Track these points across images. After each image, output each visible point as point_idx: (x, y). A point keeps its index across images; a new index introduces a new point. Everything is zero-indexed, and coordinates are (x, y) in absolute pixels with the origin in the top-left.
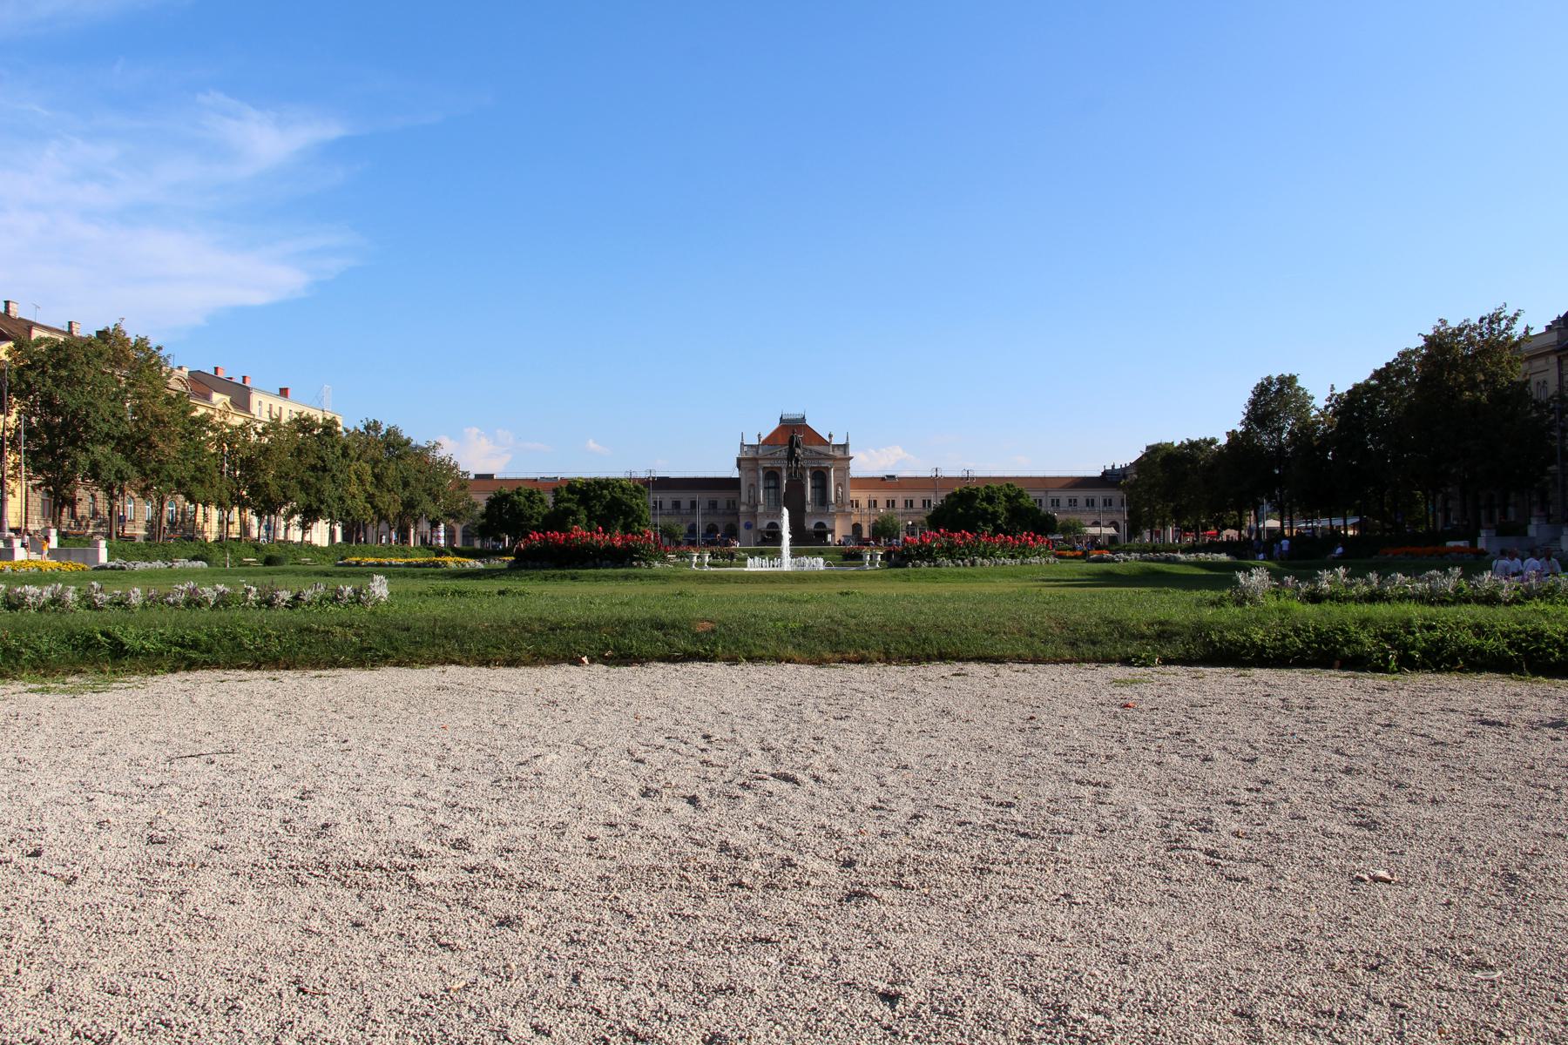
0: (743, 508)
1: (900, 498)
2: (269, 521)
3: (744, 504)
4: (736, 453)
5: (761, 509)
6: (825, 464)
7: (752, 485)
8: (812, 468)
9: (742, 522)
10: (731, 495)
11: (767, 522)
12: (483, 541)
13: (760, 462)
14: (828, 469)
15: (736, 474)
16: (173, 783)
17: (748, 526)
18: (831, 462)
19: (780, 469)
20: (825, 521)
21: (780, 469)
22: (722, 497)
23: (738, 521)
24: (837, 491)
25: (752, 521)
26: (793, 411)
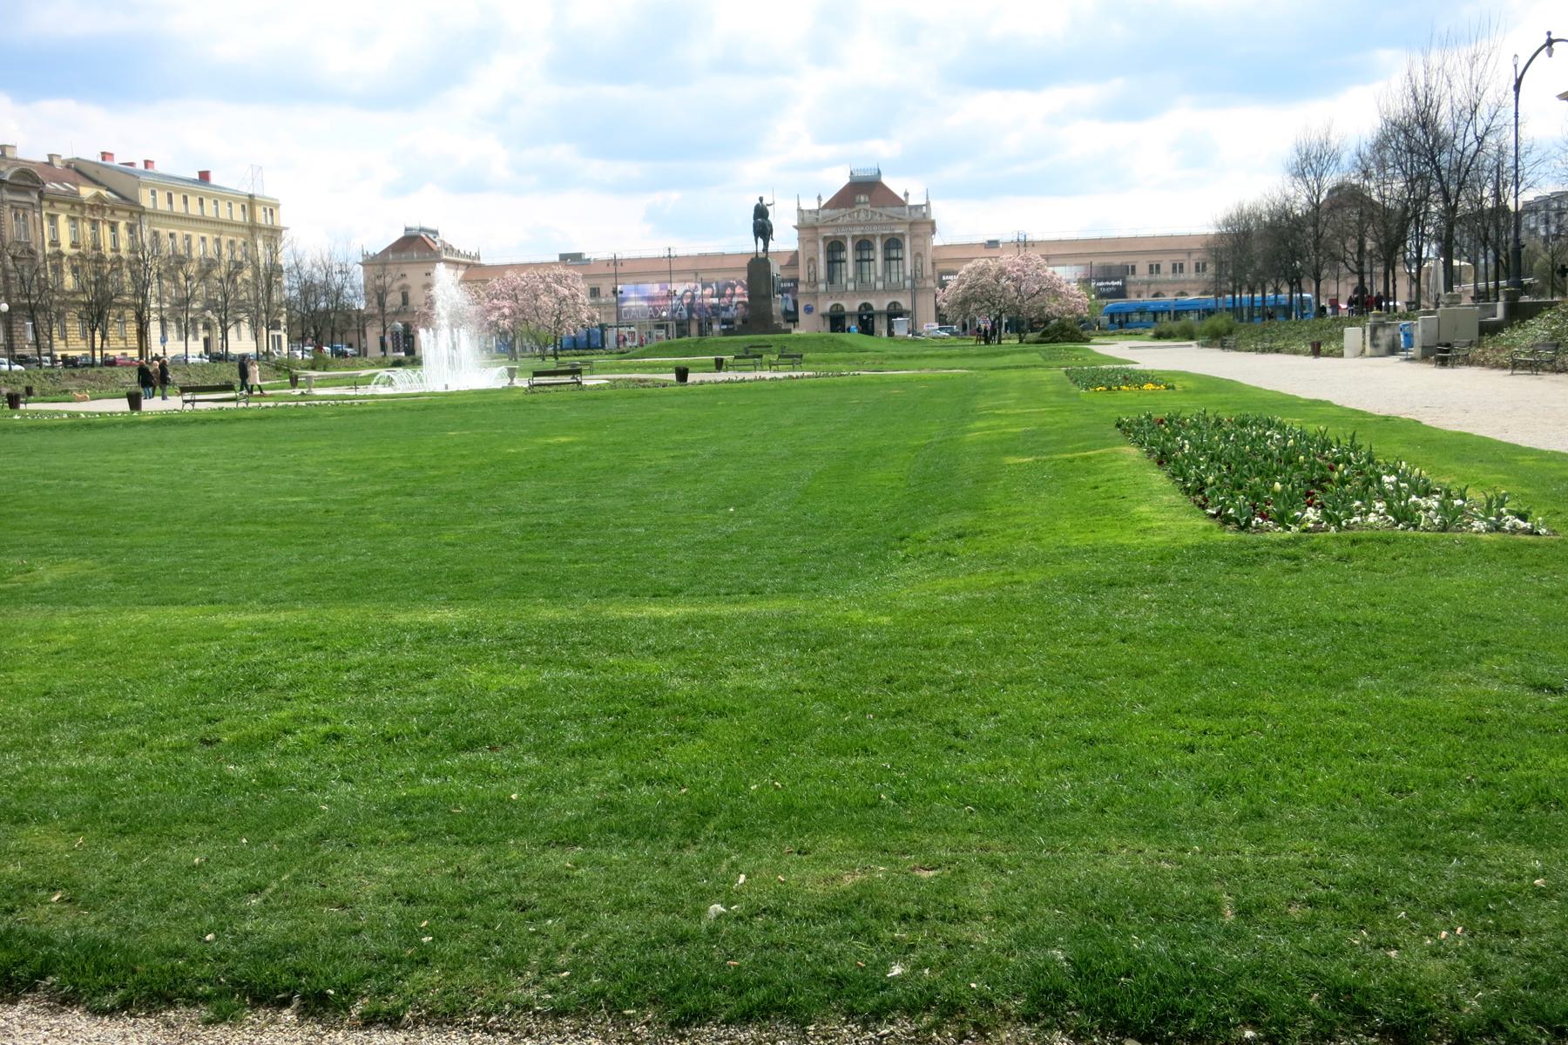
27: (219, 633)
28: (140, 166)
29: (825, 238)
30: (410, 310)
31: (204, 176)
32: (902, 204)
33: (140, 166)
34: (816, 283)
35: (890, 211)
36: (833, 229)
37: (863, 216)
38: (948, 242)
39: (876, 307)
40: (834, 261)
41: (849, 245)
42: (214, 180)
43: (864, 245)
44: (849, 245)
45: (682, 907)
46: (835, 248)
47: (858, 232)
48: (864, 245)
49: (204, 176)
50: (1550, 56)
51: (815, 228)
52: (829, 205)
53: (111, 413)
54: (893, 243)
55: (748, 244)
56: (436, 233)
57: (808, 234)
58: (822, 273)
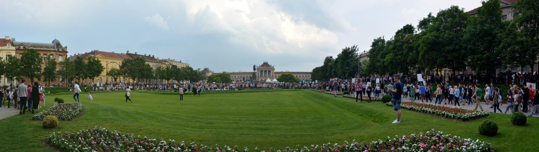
6: (270, 70)
27: (305, 133)
28: (173, 60)
30: (400, 108)
31: (180, 61)
32: (270, 66)
33: (173, 60)
34: (259, 76)
37: (265, 68)
38: (276, 71)
40: (261, 74)
41: (264, 72)
42: (182, 62)
43: (265, 71)
44: (264, 72)
45: (80, 70)
46: (262, 71)
47: (264, 70)
48: (265, 71)
49: (180, 61)
50: (430, 13)
51: (259, 69)
52: (261, 66)
53: (28, 44)
54: (269, 71)
55: (252, 71)
56: (208, 69)
57: (258, 70)
58: (260, 75)
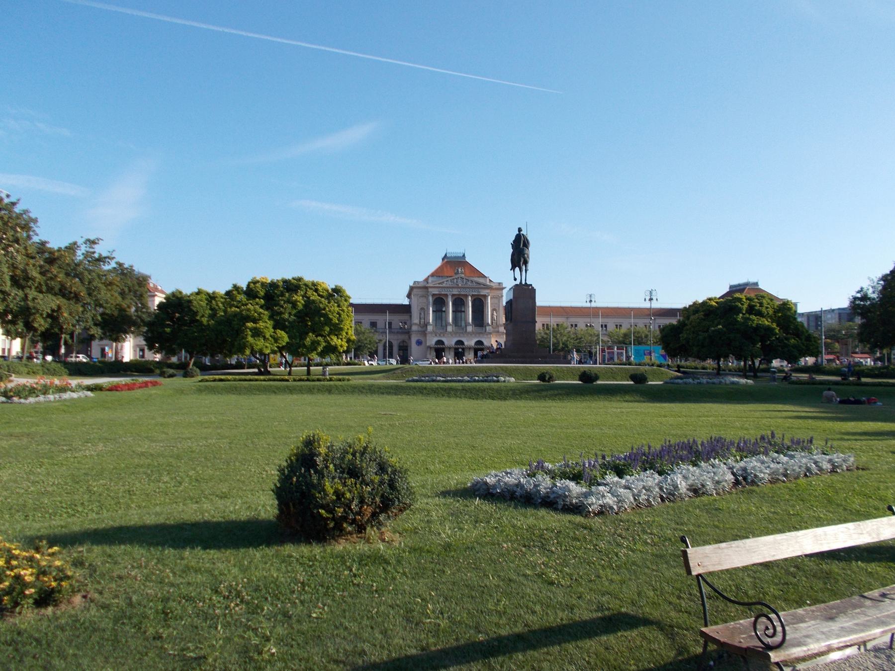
0: (414, 328)
1: (597, 323)
2: (117, 347)
3: (416, 324)
4: (694, 301)
5: (430, 328)
6: (483, 292)
7: (422, 309)
8: (453, 295)
9: (414, 339)
10: (405, 317)
11: (436, 339)
12: (212, 356)
13: (430, 290)
14: (485, 296)
15: (406, 302)
16: (67, 663)
17: (419, 343)
18: (488, 291)
19: (446, 295)
20: (444, 339)
21: (446, 295)
22: (397, 320)
23: (410, 338)
24: (492, 314)
25: (422, 339)
26: (455, 250)
29: (433, 295)
35: (476, 279)
36: (439, 289)
39: (446, 343)
43: (459, 303)
46: (439, 302)
47: (455, 292)
48: (459, 303)
